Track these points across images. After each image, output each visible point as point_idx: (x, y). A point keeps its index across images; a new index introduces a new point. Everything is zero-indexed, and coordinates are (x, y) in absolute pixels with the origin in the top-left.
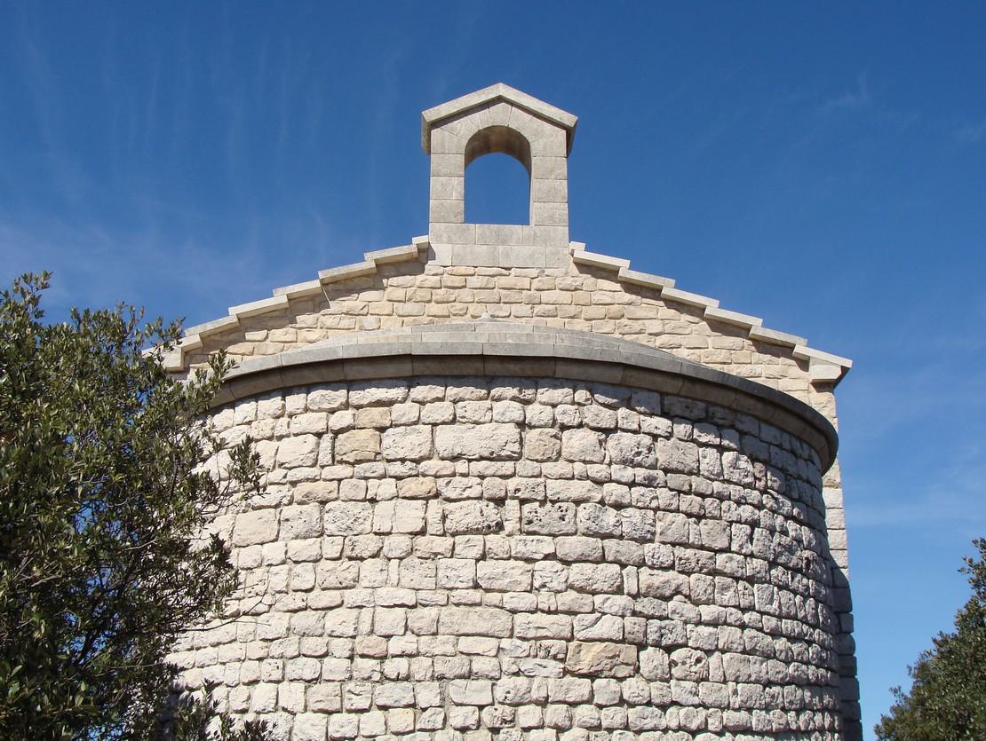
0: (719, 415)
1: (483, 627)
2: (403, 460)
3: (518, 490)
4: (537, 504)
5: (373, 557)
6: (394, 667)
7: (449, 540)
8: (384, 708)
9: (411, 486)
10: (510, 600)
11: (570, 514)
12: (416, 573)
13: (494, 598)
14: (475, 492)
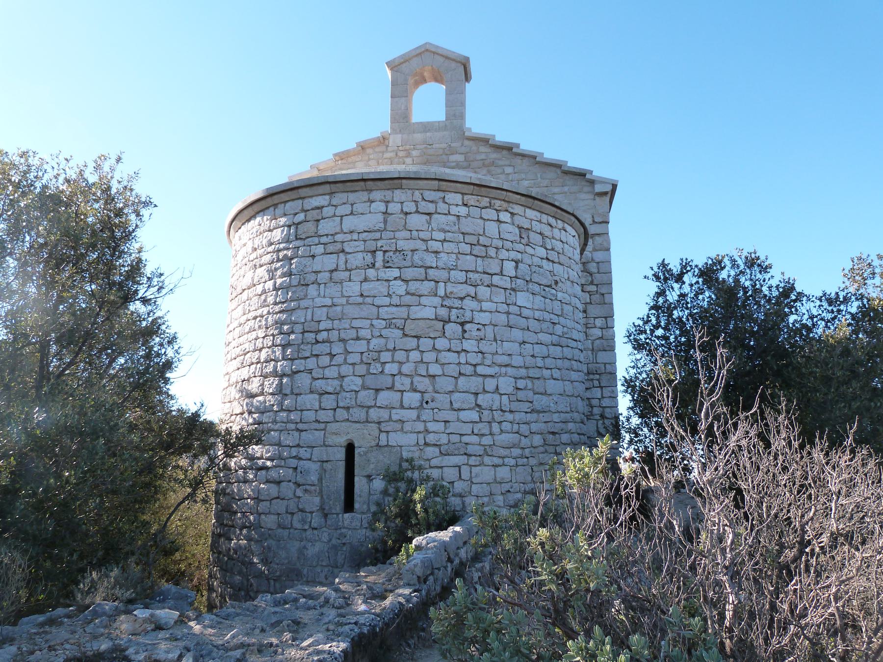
0: (497, 205)
1: (364, 314)
2: (327, 235)
3: (382, 246)
4: (392, 253)
5: (313, 283)
6: (323, 336)
7: (347, 273)
8: (317, 356)
9: (331, 248)
10: (378, 301)
11: (409, 257)
12: (333, 290)
13: (369, 300)
14: (362, 248)
